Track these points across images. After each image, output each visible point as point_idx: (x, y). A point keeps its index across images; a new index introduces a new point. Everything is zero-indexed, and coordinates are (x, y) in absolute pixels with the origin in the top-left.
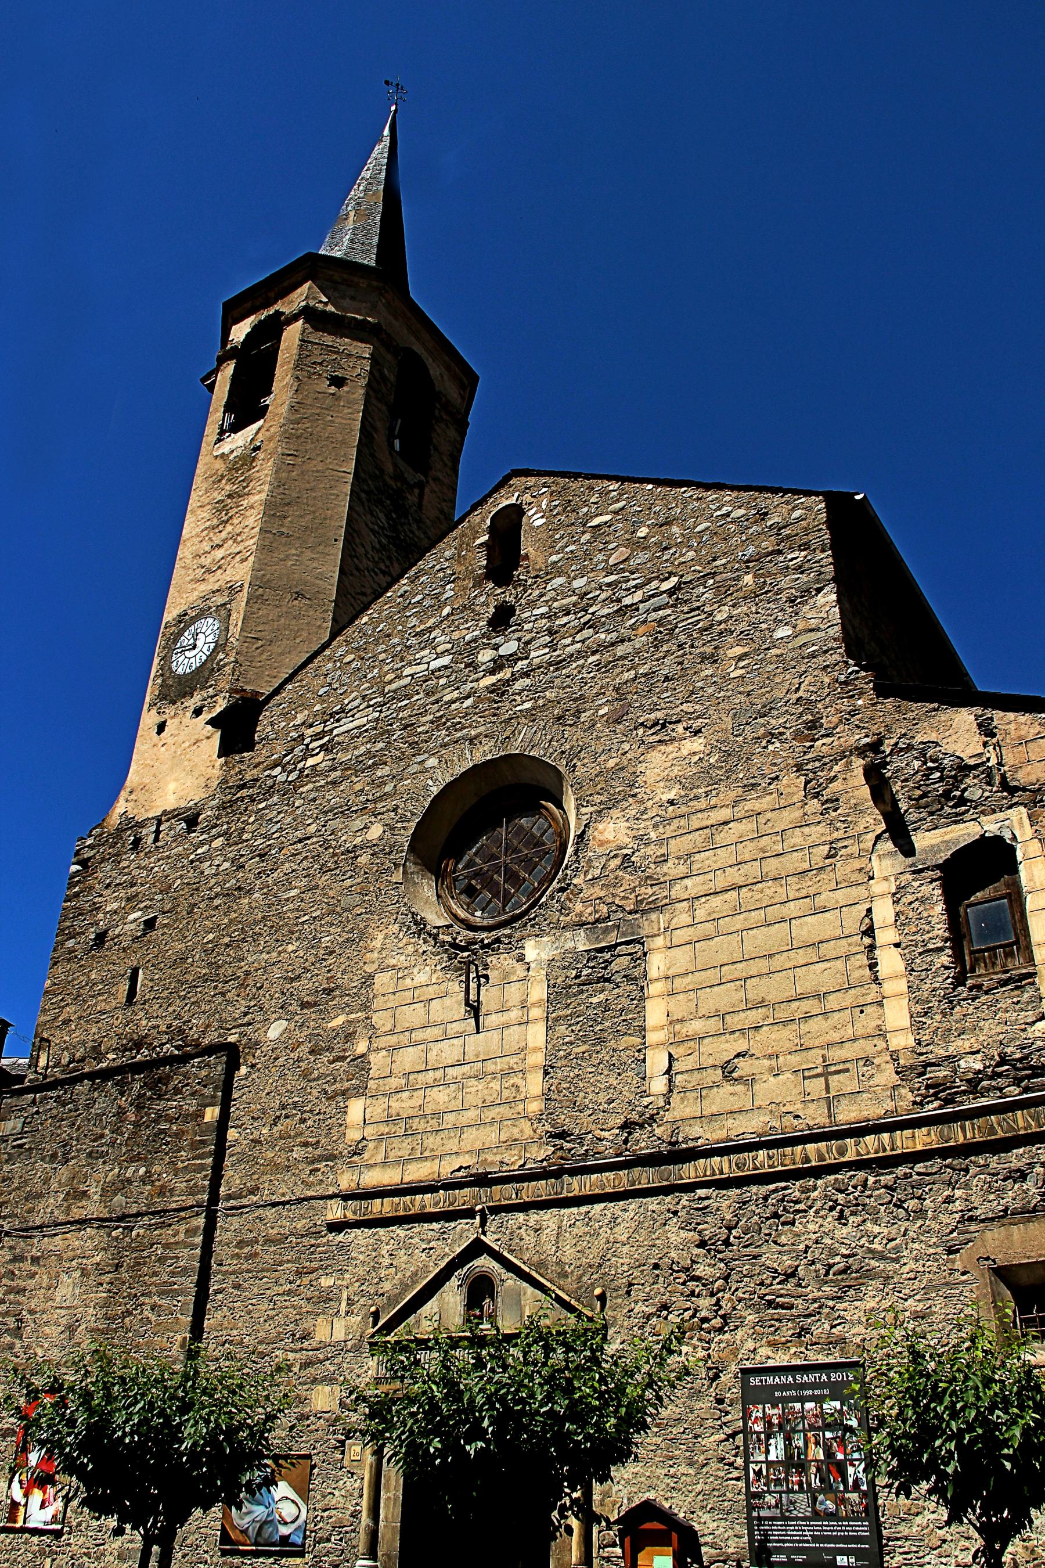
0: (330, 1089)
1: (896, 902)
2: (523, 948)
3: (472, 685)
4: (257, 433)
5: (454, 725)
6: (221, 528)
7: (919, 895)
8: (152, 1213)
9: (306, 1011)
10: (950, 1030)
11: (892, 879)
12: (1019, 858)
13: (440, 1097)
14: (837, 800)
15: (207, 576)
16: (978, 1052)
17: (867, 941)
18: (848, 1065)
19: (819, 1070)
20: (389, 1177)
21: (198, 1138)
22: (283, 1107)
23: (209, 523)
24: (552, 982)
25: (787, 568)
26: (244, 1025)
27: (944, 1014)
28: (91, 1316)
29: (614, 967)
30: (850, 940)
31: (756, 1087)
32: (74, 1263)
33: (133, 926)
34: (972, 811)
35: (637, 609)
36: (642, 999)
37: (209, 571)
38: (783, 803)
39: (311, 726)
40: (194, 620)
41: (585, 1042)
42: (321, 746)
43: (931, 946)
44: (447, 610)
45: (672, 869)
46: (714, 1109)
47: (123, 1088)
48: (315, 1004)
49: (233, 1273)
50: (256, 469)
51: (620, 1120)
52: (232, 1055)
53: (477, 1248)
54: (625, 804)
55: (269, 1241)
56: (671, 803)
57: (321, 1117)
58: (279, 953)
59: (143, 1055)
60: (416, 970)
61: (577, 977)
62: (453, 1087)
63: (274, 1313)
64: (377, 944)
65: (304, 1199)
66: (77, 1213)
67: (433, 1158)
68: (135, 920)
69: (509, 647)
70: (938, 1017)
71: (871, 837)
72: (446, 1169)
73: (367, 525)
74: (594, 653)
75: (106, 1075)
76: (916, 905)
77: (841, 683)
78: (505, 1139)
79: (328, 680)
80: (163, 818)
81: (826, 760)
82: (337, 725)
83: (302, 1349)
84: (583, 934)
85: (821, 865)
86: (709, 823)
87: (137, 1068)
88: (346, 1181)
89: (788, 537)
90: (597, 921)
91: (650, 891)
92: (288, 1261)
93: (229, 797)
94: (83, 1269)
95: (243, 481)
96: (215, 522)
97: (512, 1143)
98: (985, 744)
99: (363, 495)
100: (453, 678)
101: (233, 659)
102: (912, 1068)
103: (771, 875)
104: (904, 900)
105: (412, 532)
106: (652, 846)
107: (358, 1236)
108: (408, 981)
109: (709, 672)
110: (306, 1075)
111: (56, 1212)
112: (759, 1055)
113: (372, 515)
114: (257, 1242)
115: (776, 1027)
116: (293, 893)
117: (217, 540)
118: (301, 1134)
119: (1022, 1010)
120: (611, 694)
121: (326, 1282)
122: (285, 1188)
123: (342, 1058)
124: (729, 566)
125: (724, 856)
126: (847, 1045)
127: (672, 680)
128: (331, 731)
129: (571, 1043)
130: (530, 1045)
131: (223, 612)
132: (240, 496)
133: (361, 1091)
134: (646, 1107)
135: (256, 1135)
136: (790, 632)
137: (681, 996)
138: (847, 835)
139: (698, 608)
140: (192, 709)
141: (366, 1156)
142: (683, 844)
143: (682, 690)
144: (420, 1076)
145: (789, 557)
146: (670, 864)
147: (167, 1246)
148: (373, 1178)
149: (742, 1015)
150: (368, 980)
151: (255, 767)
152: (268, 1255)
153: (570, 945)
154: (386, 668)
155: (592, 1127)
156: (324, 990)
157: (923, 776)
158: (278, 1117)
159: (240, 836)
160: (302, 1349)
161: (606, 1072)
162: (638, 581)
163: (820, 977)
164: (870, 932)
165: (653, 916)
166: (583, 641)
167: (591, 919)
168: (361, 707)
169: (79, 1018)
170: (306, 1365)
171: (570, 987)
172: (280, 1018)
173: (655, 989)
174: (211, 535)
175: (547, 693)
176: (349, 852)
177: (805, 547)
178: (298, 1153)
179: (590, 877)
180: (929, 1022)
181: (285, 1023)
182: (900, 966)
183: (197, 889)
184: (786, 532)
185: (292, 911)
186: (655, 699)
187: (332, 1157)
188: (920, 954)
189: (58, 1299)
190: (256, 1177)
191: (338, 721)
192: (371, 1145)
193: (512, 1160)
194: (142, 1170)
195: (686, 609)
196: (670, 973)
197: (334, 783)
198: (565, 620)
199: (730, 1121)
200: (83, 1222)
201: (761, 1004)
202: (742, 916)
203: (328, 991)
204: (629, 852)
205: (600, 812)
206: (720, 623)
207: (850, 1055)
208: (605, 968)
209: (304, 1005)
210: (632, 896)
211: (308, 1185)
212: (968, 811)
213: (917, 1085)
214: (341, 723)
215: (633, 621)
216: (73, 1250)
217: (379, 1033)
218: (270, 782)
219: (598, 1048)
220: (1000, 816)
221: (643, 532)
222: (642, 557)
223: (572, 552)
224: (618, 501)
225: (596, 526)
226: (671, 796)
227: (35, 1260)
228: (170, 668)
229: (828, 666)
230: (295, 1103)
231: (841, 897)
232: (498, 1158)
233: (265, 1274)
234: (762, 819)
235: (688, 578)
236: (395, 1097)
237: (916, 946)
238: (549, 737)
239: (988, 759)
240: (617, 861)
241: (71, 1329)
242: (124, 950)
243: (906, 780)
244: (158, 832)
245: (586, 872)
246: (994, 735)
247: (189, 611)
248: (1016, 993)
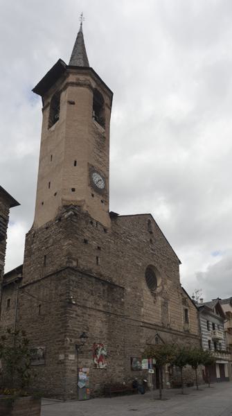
72: (153, 323)
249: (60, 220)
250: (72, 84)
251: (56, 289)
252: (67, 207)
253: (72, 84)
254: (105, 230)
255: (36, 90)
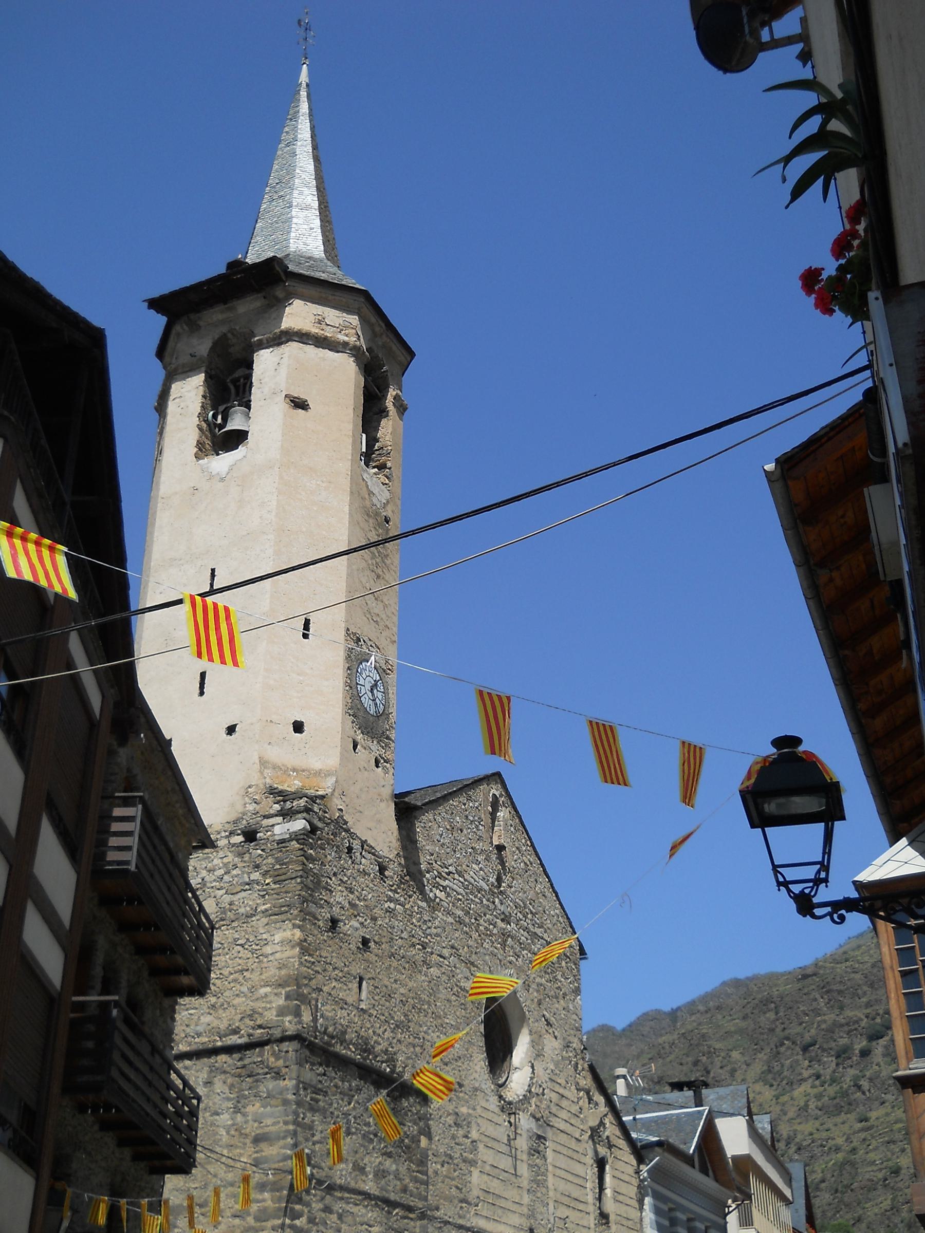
249: (250, 836)
250: (303, 337)
251: (237, 1110)
252: (286, 801)
253: (303, 337)
254: (382, 869)
255: (155, 304)
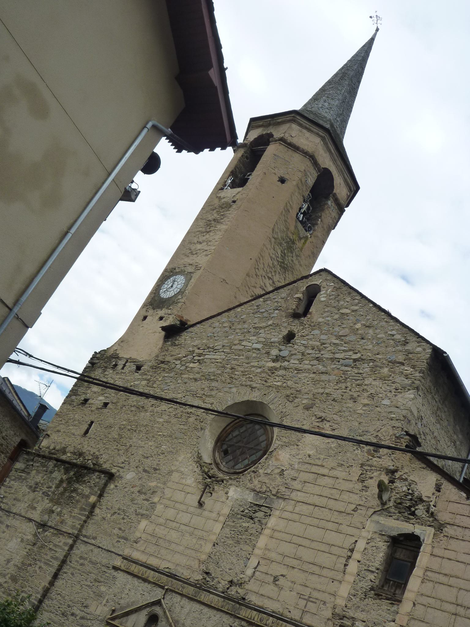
0: (138, 511)
1: (368, 543)
2: (229, 489)
3: (264, 363)
4: (237, 194)
5: (249, 378)
6: (205, 234)
7: (377, 545)
8: (56, 529)
9: (144, 473)
10: (359, 607)
11: (371, 533)
12: (421, 550)
13: (174, 535)
14: (368, 488)
15: (190, 255)
16: (364, 622)
17: (349, 554)
18: (317, 601)
19: (306, 597)
20: (143, 558)
21: (84, 506)
22: (119, 509)
23: (201, 229)
24: (233, 509)
25: (402, 373)
26: (120, 467)
27: (361, 599)
28: (17, 560)
29: (257, 514)
30: (343, 550)
31: (282, 592)
32: (20, 535)
33: (99, 402)
34: (415, 520)
35: (339, 362)
36: (260, 533)
37: (192, 253)
38: (348, 478)
39: (199, 349)
40: (177, 274)
41: (233, 540)
42: (199, 360)
43: (370, 569)
44: (270, 322)
45: (296, 485)
46: (263, 593)
47: (67, 471)
48: (149, 473)
49: (73, 568)
50: (230, 212)
51: (230, 579)
52: (110, 476)
53: (158, 603)
54: (292, 447)
55: (91, 562)
56: (309, 456)
57: (130, 521)
58: (145, 444)
59: (79, 461)
60: (189, 477)
61: (243, 511)
62: (180, 533)
63: (80, 591)
64: (180, 459)
65: (110, 551)
66: (29, 515)
67: (160, 558)
68: (101, 400)
69: (285, 353)
70: (358, 599)
71: (372, 511)
72: (163, 565)
73: (269, 254)
74: (314, 373)
75: (63, 462)
76: (374, 548)
77: (396, 437)
78: (185, 563)
79: (214, 330)
80: (129, 360)
81: (373, 468)
82: (208, 353)
83: (83, 611)
84: (252, 495)
85: (349, 512)
86: (318, 472)
87: (74, 465)
88: (127, 552)
89: (410, 359)
90: (260, 492)
91: (284, 489)
92: (94, 573)
93: (156, 364)
94: (22, 539)
95: (222, 215)
96: (204, 230)
97: (189, 568)
98: (433, 494)
99: (273, 240)
100: (259, 356)
101: (183, 301)
102: (339, 615)
103: (329, 507)
104: (371, 544)
105: (292, 261)
106: (293, 471)
107: (121, 576)
108: (184, 481)
109: (350, 405)
110: (132, 500)
111: (22, 511)
112: (288, 579)
113: (274, 249)
114: (87, 560)
115: (300, 571)
116: (161, 420)
117: (201, 240)
118: (120, 524)
119: (389, 614)
120: (310, 396)
121: (103, 589)
122: (105, 543)
123: (147, 500)
124: (381, 361)
125: (317, 490)
126: (321, 593)
127: (336, 401)
128: (205, 355)
129: (228, 538)
130: (214, 531)
131: (189, 276)
132: (218, 222)
133: (147, 517)
134: (241, 578)
135: (105, 516)
136: (388, 404)
137: (274, 540)
138: (364, 505)
139: (361, 374)
140: (159, 316)
141: (138, 545)
142: (304, 476)
143: (337, 408)
144: (171, 523)
145: (406, 369)
146: (296, 482)
147: (55, 545)
148: (136, 555)
149: (291, 560)
150: (170, 472)
151: (171, 356)
152: (89, 567)
153: (246, 497)
154: (237, 337)
155: (219, 576)
156: (154, 468)
157: (405, 495)
158: (115, 513)
159: (153, 384)
160: (83, 611)
161: (234, 556)
162: (345, 348)
163: (325, 559)
164: (352, 550)
165: (280, 501)
166: (312, 365)
167: (258, 490)
168: (220, 351)
169: (64, 432)
170: (82, 618)
171: (238, 514)
172: (134, 471)
173: (267, 532)
174: (200, 235)
175: (289, 382)
176: (188, 413)
177: (414, 367)
178: (116, 531)
179: (266, 472)
180: (354, 600)
181: (134, 474)
182: (355, 571)
183: (128, 399)
184: (410, 356)
185: (157, 428)
186: (325, 407)
187: (126, 539)
188: (365, 570)
189: (9, 547)
190: (98, 533)
191: (210, 352)
192: (142, 542)
193: (185, 573)
194: (59, 509)
195: (356, 372)
196: (275, 528)
197: (196, 380)
198: (310, 352)
199: (266, 600)
200: (30, 520)
201: (299, 559)
202: (311, 518)
203: (155, 469)
204: (284, 469)
205: (282, 446)
206: (366, 385)
207: (320, 598)
208: (254, 513)
209: (145, 471)
210: (277, 488)
211: (114, 547)
212: (413, 519)
213: (337, 623)
214: (210, 354)
215: (335, 366)
216: (22, 529)
217: (165, 497)
218: (173, 366)
219: (236, 545)
220: (424, 528)
221: (358, 326)
222: (352, 338)
223: (328, 321)
224: (356, 305)
225: (343, 314)
226: (311, 453)
227: (7, 526)
228: (159, 292)
229: (395, 427)
230: (124, 510)
231: (350, 531)
232: (182, 571)
233: (84, 574)
234: (338, 481)
235: (363, 357)
236: (159, 526)
237: (365, 565)
238: (280, 402)
239: (431, 501)
240: (279, 471)
241: (8, 561)
242: (92, 411)
243: (397, 493)
244: (124, 365)
245: (265, 469)
246: (439, 491)
247: (177, 268)
248: (391, 605)
